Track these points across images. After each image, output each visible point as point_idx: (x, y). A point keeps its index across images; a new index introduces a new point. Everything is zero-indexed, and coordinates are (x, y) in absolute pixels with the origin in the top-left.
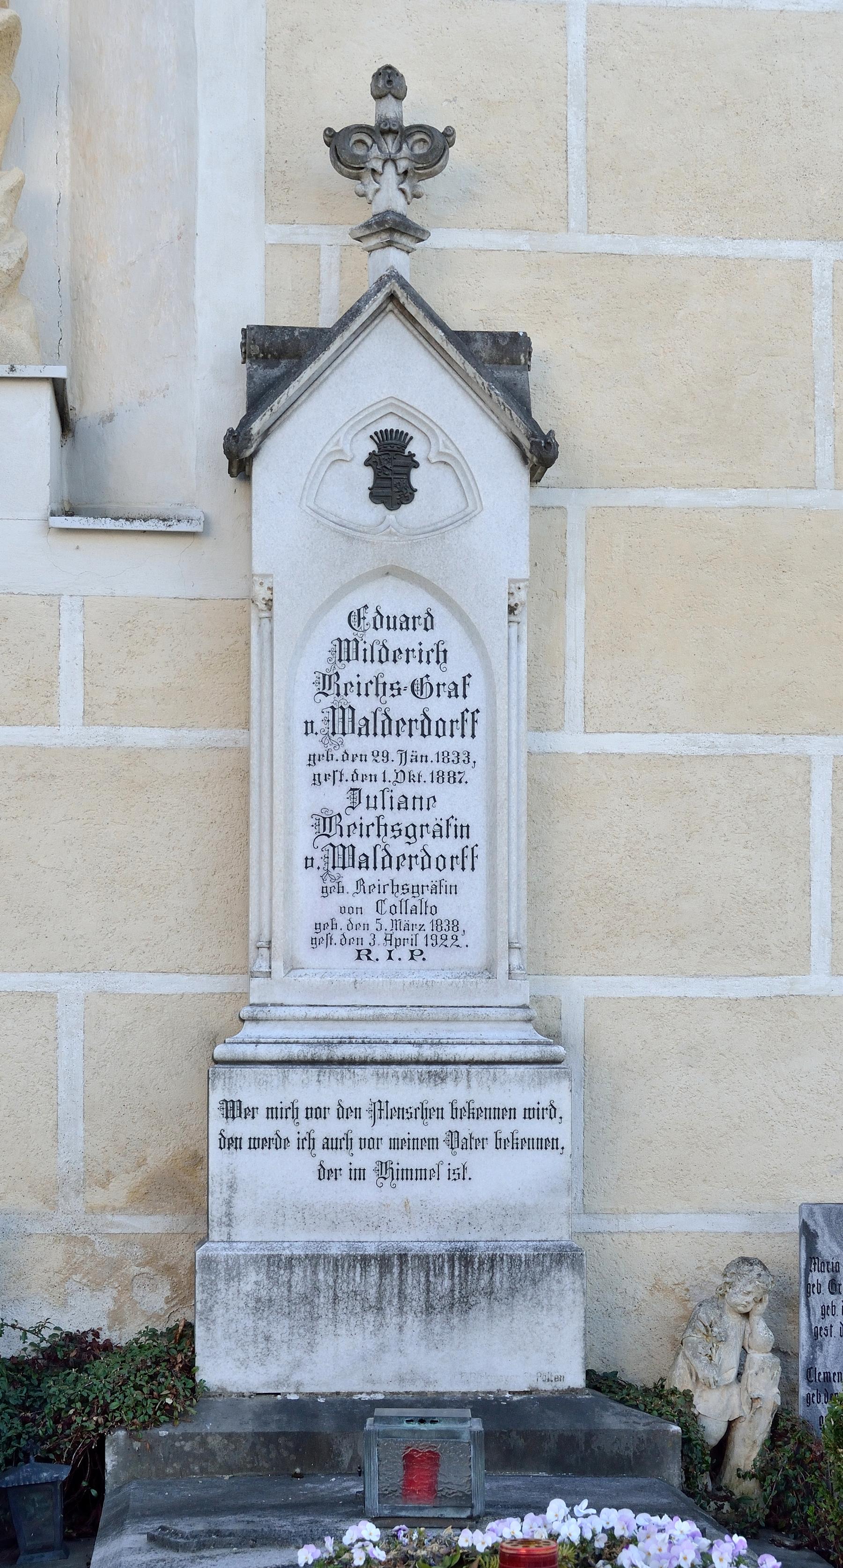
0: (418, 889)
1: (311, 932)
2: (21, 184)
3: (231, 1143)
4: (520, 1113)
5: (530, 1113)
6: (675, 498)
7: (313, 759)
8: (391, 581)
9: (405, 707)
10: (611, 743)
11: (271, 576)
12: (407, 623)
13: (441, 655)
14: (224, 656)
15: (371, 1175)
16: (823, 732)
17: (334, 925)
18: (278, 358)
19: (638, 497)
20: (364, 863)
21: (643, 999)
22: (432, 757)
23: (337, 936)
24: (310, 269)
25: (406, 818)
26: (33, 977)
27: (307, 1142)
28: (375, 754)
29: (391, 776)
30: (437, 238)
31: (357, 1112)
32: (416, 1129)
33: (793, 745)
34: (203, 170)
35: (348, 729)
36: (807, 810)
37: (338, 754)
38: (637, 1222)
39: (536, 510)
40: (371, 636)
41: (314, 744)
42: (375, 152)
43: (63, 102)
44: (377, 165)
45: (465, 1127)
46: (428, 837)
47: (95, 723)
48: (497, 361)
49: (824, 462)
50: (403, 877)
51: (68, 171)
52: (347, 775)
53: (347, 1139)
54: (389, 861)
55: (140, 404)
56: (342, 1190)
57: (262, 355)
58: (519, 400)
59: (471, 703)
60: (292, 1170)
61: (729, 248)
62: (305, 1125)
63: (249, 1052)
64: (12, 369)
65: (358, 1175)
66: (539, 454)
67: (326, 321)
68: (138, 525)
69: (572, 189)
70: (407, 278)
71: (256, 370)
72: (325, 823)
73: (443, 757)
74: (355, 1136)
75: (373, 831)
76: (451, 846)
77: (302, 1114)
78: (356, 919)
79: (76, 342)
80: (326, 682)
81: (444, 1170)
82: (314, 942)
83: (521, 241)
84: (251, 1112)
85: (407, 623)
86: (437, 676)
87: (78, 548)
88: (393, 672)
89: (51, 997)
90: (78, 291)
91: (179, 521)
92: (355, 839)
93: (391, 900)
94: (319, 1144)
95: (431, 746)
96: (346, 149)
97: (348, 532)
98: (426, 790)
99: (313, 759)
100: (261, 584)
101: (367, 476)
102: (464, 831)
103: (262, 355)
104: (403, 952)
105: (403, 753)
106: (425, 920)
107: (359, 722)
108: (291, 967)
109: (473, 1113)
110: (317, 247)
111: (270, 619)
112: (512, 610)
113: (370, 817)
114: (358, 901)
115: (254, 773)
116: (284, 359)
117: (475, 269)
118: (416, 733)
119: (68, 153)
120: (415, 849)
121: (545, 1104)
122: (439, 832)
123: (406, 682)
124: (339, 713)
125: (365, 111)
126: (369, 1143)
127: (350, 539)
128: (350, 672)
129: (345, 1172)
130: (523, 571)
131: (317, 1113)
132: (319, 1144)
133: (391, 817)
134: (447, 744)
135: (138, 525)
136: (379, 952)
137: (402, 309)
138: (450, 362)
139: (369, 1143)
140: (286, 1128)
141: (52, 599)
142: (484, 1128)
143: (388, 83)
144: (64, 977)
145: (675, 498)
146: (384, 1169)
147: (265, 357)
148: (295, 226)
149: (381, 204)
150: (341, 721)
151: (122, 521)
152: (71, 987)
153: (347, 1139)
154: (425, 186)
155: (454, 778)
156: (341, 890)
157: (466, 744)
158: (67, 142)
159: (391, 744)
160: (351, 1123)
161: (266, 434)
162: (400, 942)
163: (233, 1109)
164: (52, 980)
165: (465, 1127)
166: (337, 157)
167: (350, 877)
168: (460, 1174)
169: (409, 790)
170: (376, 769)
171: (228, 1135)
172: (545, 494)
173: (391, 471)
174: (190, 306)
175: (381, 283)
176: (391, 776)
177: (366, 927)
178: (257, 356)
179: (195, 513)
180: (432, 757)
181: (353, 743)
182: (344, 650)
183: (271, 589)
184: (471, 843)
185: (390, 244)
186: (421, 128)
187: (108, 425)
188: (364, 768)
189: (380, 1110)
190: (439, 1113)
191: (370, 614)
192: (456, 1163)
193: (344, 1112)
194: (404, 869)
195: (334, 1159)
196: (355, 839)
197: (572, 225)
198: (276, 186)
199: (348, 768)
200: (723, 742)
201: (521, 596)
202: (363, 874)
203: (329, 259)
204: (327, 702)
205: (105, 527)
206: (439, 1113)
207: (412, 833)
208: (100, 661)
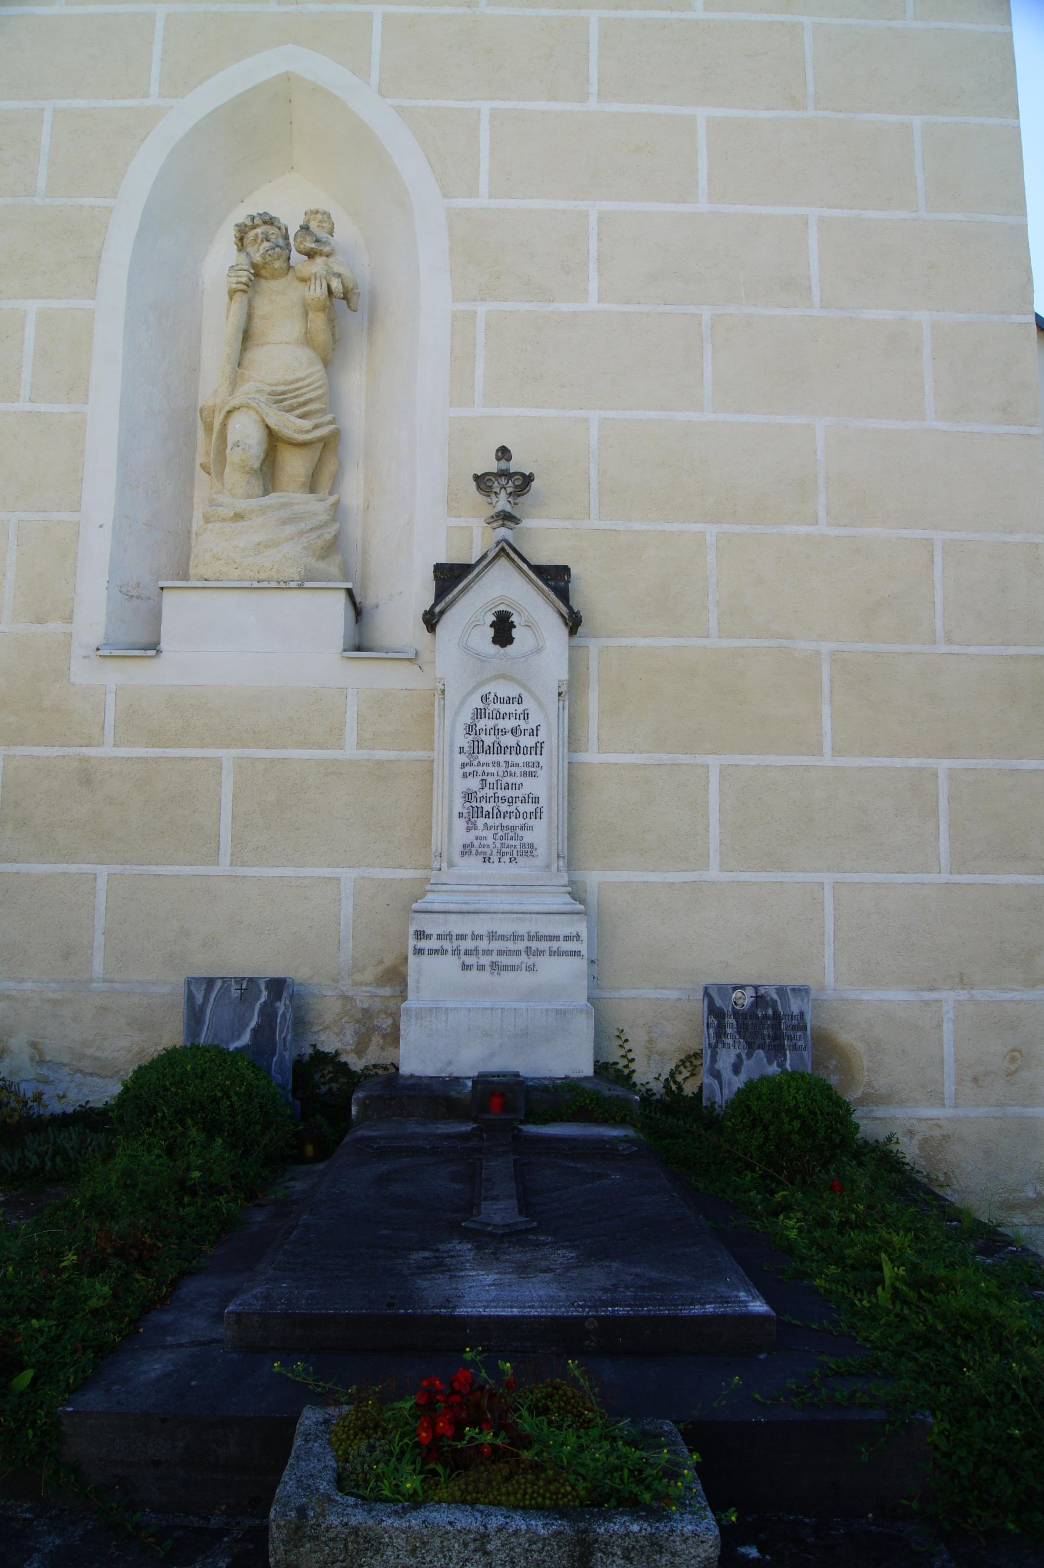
0: (513, 828)
1: (461, 848)
2: (338, 502)
3: (419, 952)
4: (562, 938)
5: (567, 938)
6: (641, 642)
7: (463, 765)
8: (502, 681)
9: (509, 740)
10: (612, 758)
12: (510, 700)
13: (526, 716)
15: (488, 968)
16: (715, 753)
17: (472, 846)
18: (450, 577)
19: (623, 642)
20: (488, 815)
21: (627, 882)
22: (521, 764)
23: (474, 851)
24: (470, 536)
25: (509, 793)
26: (329, 870)
27: (456, 952)
28: (493, 763)
29: (501, 774)
30: (526, 523)
31: (481, 937)
32: (510, 945)
33: (700, 759)
35: (480, 750)
36: (707, 791)
37: (476, 763)
38: (625, 993)
39: (571, 648)
40: (492, 707)
41: (464, 758)
42: (496, 484)
44: (498, 490)
45: (535, 945)
46: (519, 803)
47: (362, 748)
48: (555, 579)
49: (713, 625)
50: (506, 822)
52: (480, 773)
53: (476, 950)
54: (500, 814)
56: (473, 975)
58: (563, 594)
59: (540, 739)
60: (449, 964)
61: (667, 527)
62: (456, 943)
63: (430, 907)
65: (481, 968)
66: (573, 622)
67: (473, 562)
69: (592, 500)
70: (511, 541)
72: (469, 796)
73: (526, 764)
74: (480, 949)
75: (492, 800)
76: (530, 807)
77: (454, 938)
78: (483, 842)
80: (470, 728)
81: (524, 966)
82: (463, 854)
83: (568, 524)
84: (429, 937)
85: (510, 700)
86: (523, 726)
88: (502, 724)
89: (338, 879)
92: (483, 804)
93: (500, 833)
94: (462, 953)
95: (521, 759)
96: (482, 481)
97: (481, 658)
98: (518, 780)
99: (463, 765)
101: (491, 632)
102: (536, 800)
104: (506, 859)
105: (507, 762)
106: (517, 843)
107: (486, 748)
108: (451, 865)
109: (539, 937)
110: (472, 528)
112: (560, 694)
113: (490, 793)
114: (484, 834)
115: (435, 772)
117: (547, 536)
118: (514, 753)
120: (513, 809)
121: (574, 934)
122: (524, 801)
123: (509, 728)
124: (476, 743)
125: (492, 466)
126: (487, 952)
127: (482, 661)
128: (481, 724)
129: (475, 967)
130: (565, 676)
131: (462, 937)
132: (462, 953)
133: (501, 793)
134: (529, 758)
136: (495, 858)
137: (508, 555)
138: (531, 580)
139: (487, 952)
140: (447, 945)
142: (544, 945)
143: (504, 453)
144: (345, 870)
145: (641, 642)
146: (494, 965)
149: (499, 507)
150: (477, 747)
152: (348, 875)
153: (476, 950)
154: (519, 500)
155: (532, 774)
156: (476, 828)
157: (538, 758)
159: (501, 758)
160: (479, 943)
161: (442, 612)
162: (504, 854)
163: (420, 935)
164: (337, 872)
165: (535, 945)
166: (479, 487)
167: (480, 822)
168: (532, 968)
169: (510, 780)
170: (494, 770)
171: (418, 947)
172: (577, 640)
173: (503, 630)
175: (498, 543)
176: (501, 774)
177: (488, 846)
180: (521, 764)
181: (483, 758)
182: (479, 714)
184: (540, 806)
185: (503, 525)
186: (516, 473)
188: (487, 770)
189: (492, 936)
190: (522, 938)
191: (492, 696)
192: (530, 963)
193: (475, 937)
194: (507, 818)
195: (470, 960)
196: (483, 804)
197: (592, 516)
199: (480, 769)
200: (665, 758)
201: (564, 689)
202: (487, 820)
203: (477, 533)
204: (471, 738)
206: (522, 938)
207: (511, 801)
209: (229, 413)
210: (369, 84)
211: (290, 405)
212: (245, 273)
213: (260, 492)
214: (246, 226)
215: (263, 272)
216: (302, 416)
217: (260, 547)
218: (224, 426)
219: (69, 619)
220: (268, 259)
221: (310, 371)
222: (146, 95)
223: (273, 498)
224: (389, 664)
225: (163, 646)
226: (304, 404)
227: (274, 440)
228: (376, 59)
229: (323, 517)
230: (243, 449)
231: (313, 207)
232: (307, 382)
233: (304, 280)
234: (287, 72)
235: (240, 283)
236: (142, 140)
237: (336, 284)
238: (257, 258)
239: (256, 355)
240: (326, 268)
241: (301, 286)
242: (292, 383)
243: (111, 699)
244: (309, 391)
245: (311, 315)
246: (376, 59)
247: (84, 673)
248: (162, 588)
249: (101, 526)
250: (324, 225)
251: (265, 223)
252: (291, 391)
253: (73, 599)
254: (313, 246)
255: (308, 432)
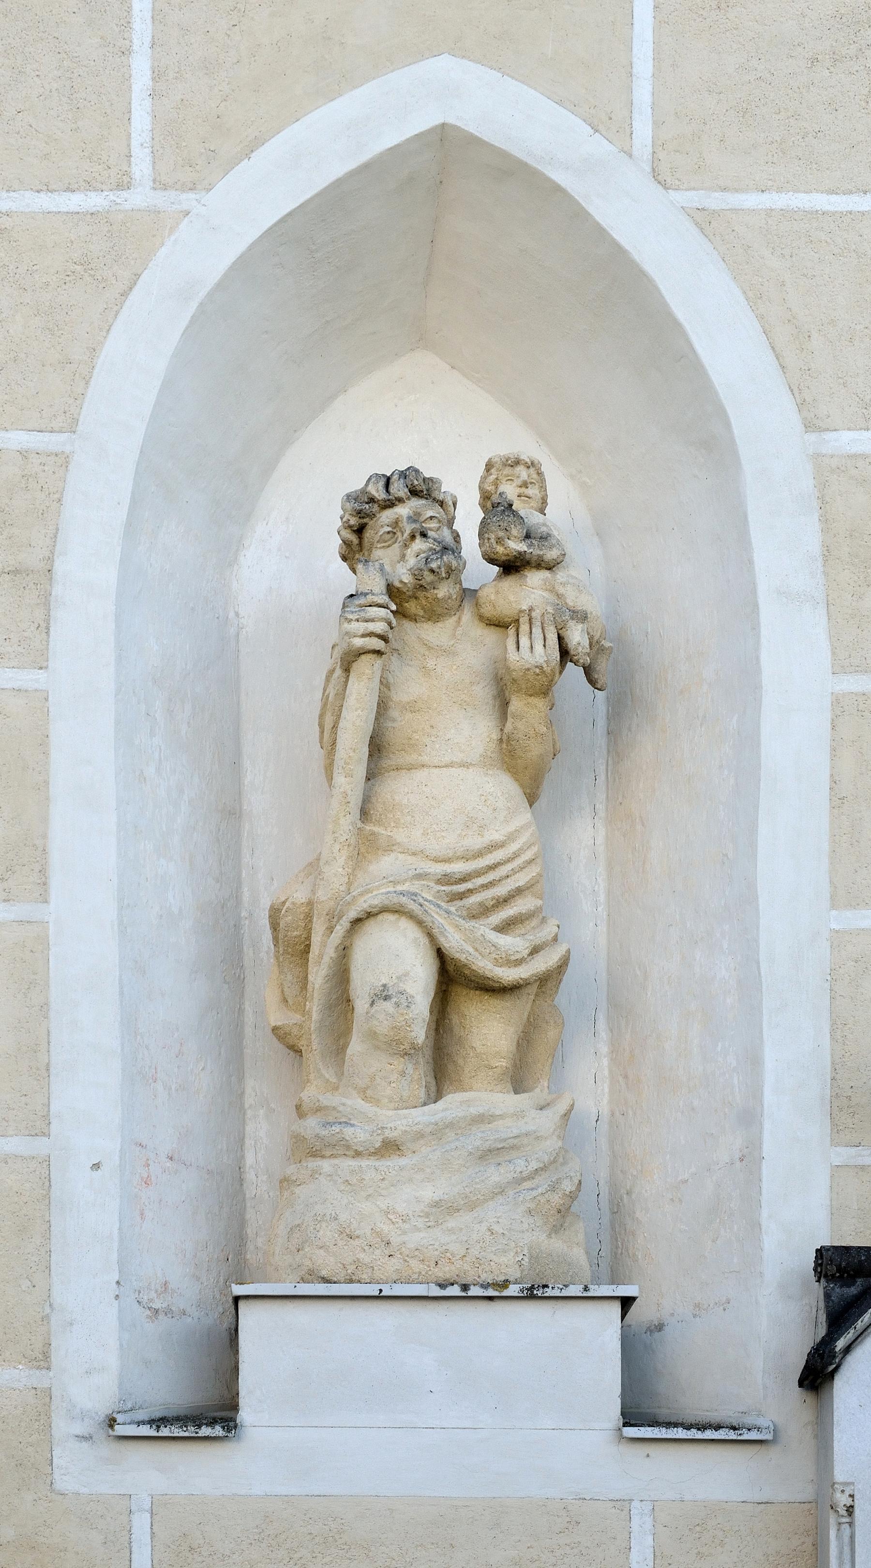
11: (853, 1484)
14: (791, 1556)
34: (769, 1097)
43: (602, 1024)
51: (606, 1090)
55: (695, 1316)
57: (838, 1275)
64: (586, 1289)
68: (709, 1434)
71: (833, 1289)
79: (616, 1254)
87: (648, 1456)
90: (618, 1205)
91: (749, 1430)
100: (843, 1491)
103: (838, 1275)
111: (851, 1524)
116: (860, 1277)
119: (606, 1073)
135: (721, 1434)
141: (623, 1504)
147: (841, 1277)
148: (860, 1148)
151: (694, 1431)
158: (605, 1062)
161: (848, 1350)
174: (755, 1226)
178: (833, 1276)
179: (762, 1422)
183: (852, 1496)
187: (657, 1335)
198: (841, 1110)
205: (677, 1437)
208: (670, 1562)
209: (357, 922)
210: (631, 156)
211: (481, 904)
212: (382, 612)
213: (422, 1094)
214: (372, 500)
215: (412, 607)
216: (504, 928)
217: (443, 1209)
218: (344, 952)
219: (43, 1359)
220: (429, 577)
221: (511, 828)
222: (124, 184)
223: (452, 1105)
224: (672, 1448)
225: (245, 1415)
226: (505, 901)
227: (452, 979)
228: (643, 92)
229: (552, 1144)
230: (397, 1005)
231: (502, 449)
232: (513, 847)
233: (499, 624)
234: (443, 125)
235: (371, 634)
236: (125, 294)
237: (577, 637)
238: (403, 575)
239: (399, 789)
240: (552, 598)
241: (491, 636)
242: (479, 854)
243: (141, 1524)
244: (514, 872)
245: (516, 704)
246: (643, 92)
247: (81, 1469)
248: (237, 1299)
249: (96, 1166)
250: (530, 491)
251: (414, 493)
252: (478, 873)
253: (46, 1318)
254: (522, 547)
255: (519, 962)
